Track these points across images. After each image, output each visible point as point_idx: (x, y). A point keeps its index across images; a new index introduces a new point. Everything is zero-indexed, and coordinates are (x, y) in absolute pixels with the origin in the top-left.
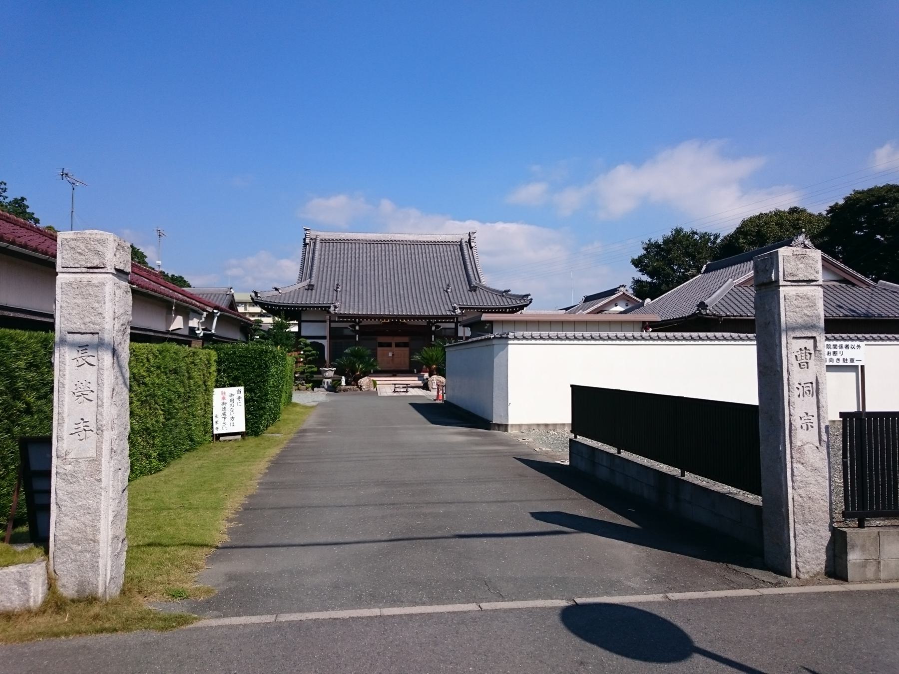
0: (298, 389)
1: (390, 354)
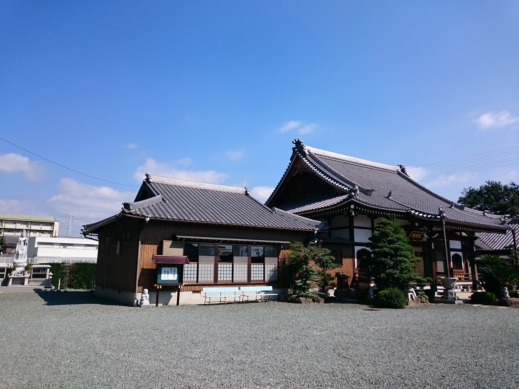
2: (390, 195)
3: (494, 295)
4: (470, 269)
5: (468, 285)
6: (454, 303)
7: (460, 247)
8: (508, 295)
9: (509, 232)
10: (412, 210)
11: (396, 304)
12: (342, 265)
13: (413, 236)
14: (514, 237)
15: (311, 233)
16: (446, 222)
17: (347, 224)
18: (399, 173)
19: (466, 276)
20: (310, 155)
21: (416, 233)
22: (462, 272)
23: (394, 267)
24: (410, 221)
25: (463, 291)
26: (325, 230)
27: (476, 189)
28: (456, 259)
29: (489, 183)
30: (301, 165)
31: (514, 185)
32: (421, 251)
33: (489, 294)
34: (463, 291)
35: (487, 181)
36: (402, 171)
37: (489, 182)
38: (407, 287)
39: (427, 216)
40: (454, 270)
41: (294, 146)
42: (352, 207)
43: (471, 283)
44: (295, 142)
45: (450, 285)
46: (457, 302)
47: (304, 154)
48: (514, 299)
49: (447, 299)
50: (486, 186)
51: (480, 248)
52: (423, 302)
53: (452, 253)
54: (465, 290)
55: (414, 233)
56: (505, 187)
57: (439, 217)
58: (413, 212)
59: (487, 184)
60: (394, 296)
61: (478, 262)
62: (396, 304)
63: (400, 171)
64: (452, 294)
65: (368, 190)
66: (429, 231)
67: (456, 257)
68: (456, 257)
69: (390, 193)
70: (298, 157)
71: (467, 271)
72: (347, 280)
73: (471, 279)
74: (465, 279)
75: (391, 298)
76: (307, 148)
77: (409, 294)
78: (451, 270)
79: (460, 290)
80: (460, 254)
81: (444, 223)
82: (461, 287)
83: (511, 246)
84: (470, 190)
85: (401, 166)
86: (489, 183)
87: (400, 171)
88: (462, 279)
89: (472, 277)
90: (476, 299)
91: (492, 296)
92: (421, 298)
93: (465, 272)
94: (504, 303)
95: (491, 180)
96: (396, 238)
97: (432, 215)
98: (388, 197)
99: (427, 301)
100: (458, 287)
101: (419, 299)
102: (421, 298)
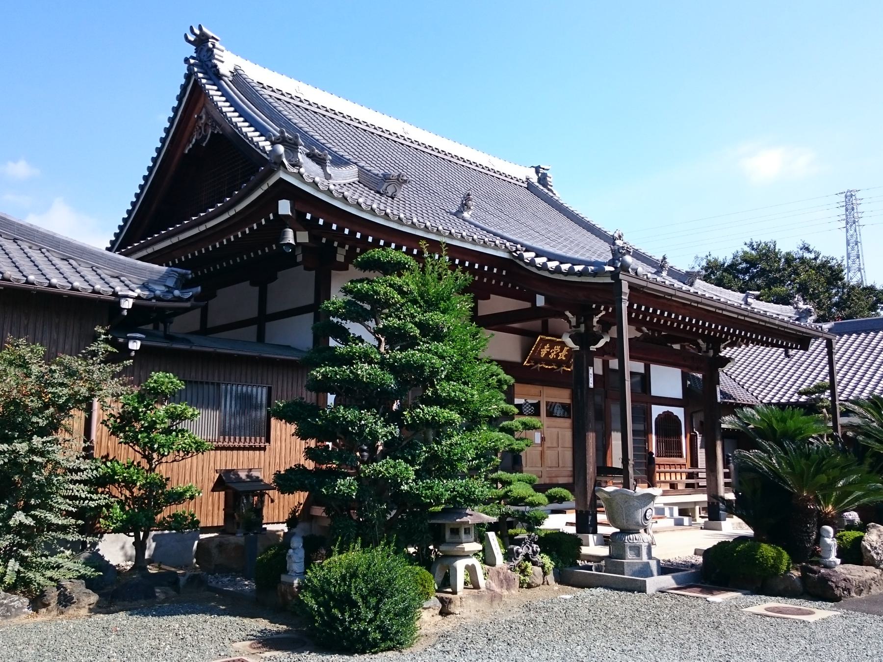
2: (465, 206)
3: (786, 556)
4: (701, 454)
5: (696, 503)
6: (642, 589)
7: (677, 392)
8: (833, 558)
9: (817, 346)
10: (528, 249)
11: (365, 632)
12: (268, 440)
13: (543, 353)
14: (831, 363)
15: (112, 305)
16: (631, 287)
17: (308, 298)
18: (530, 187)
19: (690, 476)
20: (237, 77)
21: (553, 344)
22: (681, 465)
23: (393, 449)
24: (499, 277)
25: (679, 523)
26: (179, 299)
27: (721, 260)
28: (668, 425)
29: (751, 245)
30: (207, 113)
31: (807, 249)
32: (568, 401)
33: (767, 550)
34: (679, 523)
35: (748, 242)
36: (539, 182)
37: (751, 245)
38: (455, 531)
39: (571, 269)
40: (658, 460)
41: (191, 51)
42: (284, 207)
43: (704, 497)
44: (192, 38)
45: (630, 515)
46: (655, 583)
47: (215, 76)
48: (856, 572)
49: (618, 575)
50: (745, 253)
51: (730, 397)
52: (530, 586)
53: (657, 410)
54: (686, 520)
55: (544, 342)
56: (789, 259)
57: (608, 268)
58: (529, 256)
59: (747, 249)
60: (357, 589)
61: (727, 435)
62: (365, 632)
63: (534, 179)
64: (637, 550)
65: (386, 178)
66: (582, 328)
67: (668, 420)
68: (668, 420)
69: (467, 197)
70: (197, 82)
71: (694, 463)
72: (262, 502)
73: (703, 483)
74: (688, 486)
75: (345, 601)
76: (227, 62)
77: (460, 565)
78: (650, 461)
79: (671, 522)
80: (679, 412)
81: (625, 289)
82: (676, 510)
83: (820, 389)
84: (709, 262)
85: (537, 169)
86: (751, 245)
87: (534, 179)
88: (681, 487)
89: (708, 479)
90: (717, 571)
91: (779, 557)
92: (523, 571)
93: (688, 465)
94: (821, 590)
95: (756, 239)
96: (419, 325)
97: (587, 263)
98: (458, 214)
99: (550, 577)
100: (667, 512)
101: (517, 575)
102: (523, 571)
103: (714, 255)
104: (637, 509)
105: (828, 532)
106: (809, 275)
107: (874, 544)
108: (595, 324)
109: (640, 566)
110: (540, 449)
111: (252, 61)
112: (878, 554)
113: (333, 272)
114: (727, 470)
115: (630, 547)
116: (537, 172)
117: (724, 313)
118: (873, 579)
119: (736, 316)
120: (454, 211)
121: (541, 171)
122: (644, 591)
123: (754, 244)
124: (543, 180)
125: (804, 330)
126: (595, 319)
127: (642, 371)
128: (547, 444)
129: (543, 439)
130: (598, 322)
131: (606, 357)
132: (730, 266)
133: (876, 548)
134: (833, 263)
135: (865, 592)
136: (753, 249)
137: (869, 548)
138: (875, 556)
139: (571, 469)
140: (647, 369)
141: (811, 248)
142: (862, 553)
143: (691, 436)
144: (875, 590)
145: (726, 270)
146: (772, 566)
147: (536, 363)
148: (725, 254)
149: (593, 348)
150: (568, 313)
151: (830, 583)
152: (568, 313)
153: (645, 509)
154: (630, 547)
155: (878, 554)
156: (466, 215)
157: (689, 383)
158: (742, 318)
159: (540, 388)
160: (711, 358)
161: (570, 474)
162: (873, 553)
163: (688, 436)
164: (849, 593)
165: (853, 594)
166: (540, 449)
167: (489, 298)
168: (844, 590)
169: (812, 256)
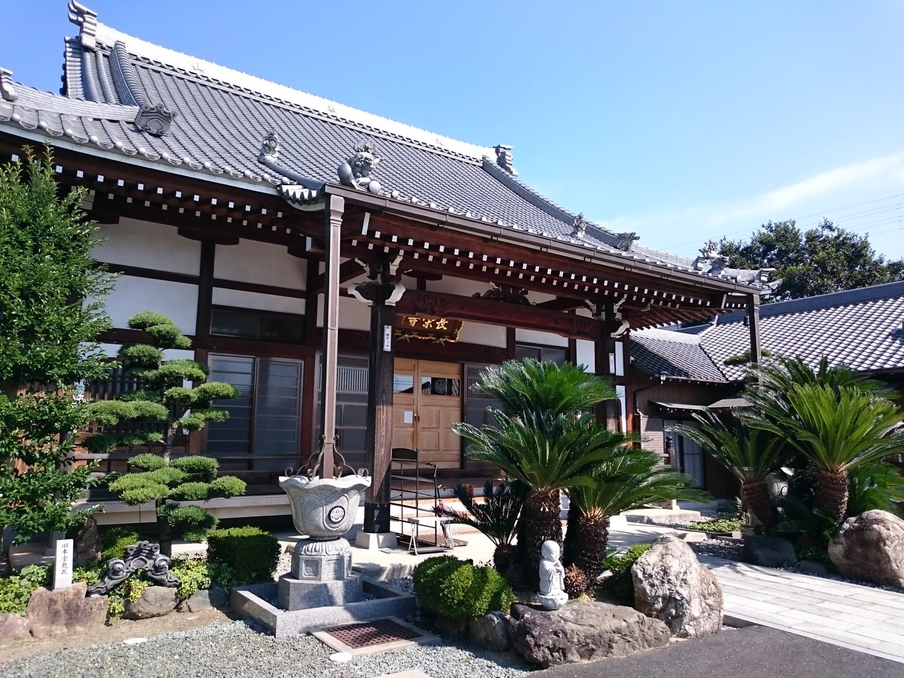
0: (130, 615)
1: (408, 417)
18: (486, 166)
31: (830, 228)
35: (766, 224)
37: (770, 226)
59: (764, 231)
63: (493, 158)
85: (497, 149)
87: (493, 158)
103: (729, 239)
104: (316, 507)
105: (550, 551)
106: (829, 253)
107: (649, 569)
108: (615, 311)
109: (311, 589)
110: (412, 429)
111: (422, 128)
112: (652, 585)
113: (217, 246)
114: (667, 455)
115: (307, 561)
116: (497, 152)
117: (633, 270)
118: (618, 631)
119: (582, 258)
120: (570, 232)
121: (501, 150)
122: (274, 634)
123: (773, 225)
124: (502, 161)
125: (703, 280)
126: (616, 307)
127: (301, 310)
128: (420, 424)
129: (416, 419)
130: (619, 310)
131: (573, 337)
132: (746, 249)
133: (651, 576)
134: (856, 240)
135: (600, 652)
136: (771, 231)
137: (640, 575)
138: (648, 588)
139: (458, 453)
140: (572, 344)
141: (834, 226)
142: (632, 583)
143: (634, 417)
144: (619, 653)
145: (742, 254)
146: (461, 603)
147: (403, 333)
148: (744, 238)
149: (613, 335)
150: (587, 301)
151: (528, 638)
152: (587, 301)
153: (329, 508)
154: (307, 561)
155: (652, 585)
156: (271, 158)
157: (632, 358)
158: (629, 269)
159: (414, 361)
160: (602, 322)
161: (457, 458)
162: (645, 584)
163: (631, 416)
164: (565, 656)
165: (574, 657)
166: (412, 429)
167: (117, 222)
168: (551, 650)
169: (835, 234)
